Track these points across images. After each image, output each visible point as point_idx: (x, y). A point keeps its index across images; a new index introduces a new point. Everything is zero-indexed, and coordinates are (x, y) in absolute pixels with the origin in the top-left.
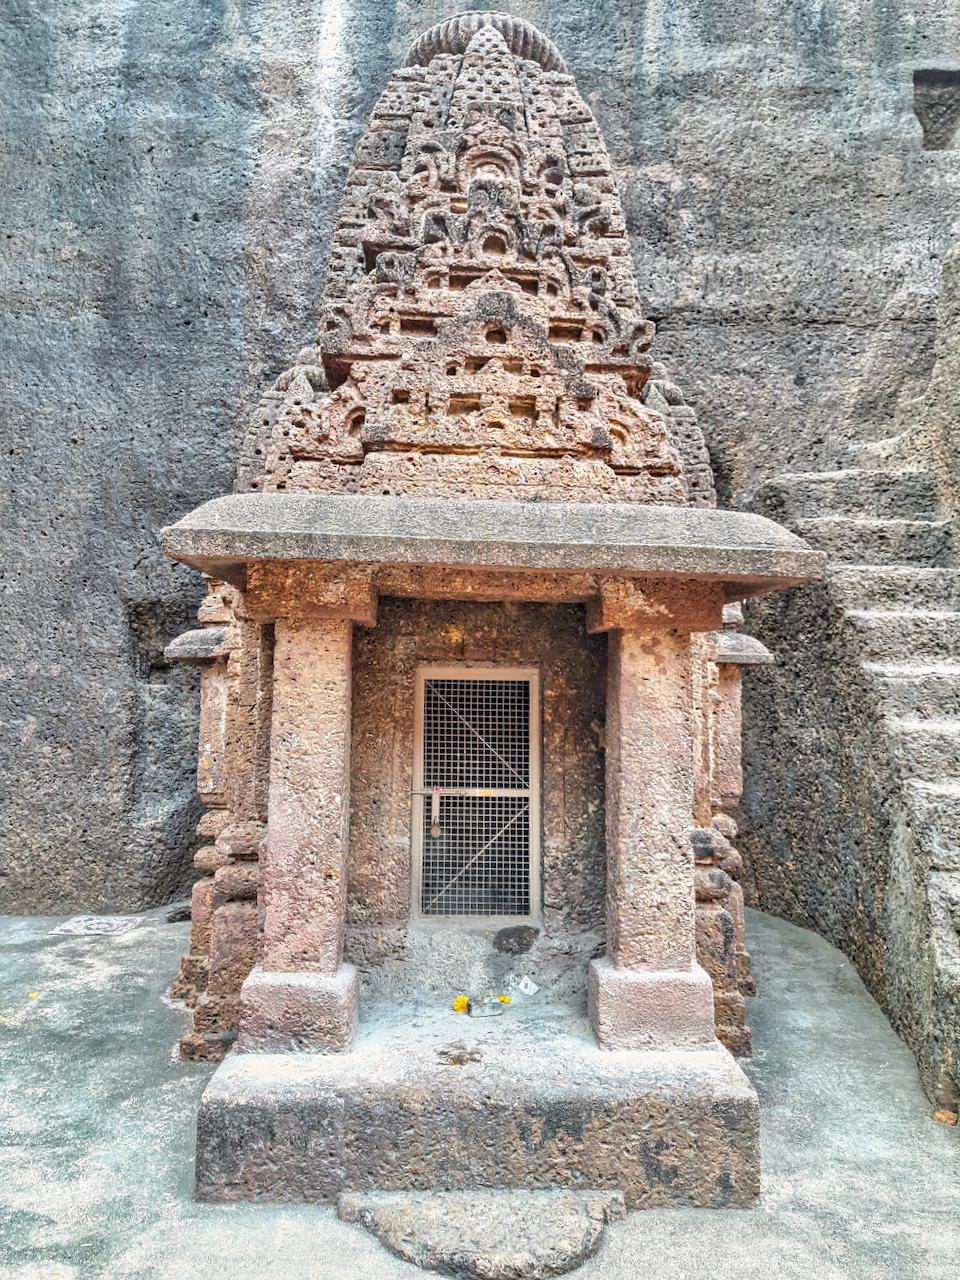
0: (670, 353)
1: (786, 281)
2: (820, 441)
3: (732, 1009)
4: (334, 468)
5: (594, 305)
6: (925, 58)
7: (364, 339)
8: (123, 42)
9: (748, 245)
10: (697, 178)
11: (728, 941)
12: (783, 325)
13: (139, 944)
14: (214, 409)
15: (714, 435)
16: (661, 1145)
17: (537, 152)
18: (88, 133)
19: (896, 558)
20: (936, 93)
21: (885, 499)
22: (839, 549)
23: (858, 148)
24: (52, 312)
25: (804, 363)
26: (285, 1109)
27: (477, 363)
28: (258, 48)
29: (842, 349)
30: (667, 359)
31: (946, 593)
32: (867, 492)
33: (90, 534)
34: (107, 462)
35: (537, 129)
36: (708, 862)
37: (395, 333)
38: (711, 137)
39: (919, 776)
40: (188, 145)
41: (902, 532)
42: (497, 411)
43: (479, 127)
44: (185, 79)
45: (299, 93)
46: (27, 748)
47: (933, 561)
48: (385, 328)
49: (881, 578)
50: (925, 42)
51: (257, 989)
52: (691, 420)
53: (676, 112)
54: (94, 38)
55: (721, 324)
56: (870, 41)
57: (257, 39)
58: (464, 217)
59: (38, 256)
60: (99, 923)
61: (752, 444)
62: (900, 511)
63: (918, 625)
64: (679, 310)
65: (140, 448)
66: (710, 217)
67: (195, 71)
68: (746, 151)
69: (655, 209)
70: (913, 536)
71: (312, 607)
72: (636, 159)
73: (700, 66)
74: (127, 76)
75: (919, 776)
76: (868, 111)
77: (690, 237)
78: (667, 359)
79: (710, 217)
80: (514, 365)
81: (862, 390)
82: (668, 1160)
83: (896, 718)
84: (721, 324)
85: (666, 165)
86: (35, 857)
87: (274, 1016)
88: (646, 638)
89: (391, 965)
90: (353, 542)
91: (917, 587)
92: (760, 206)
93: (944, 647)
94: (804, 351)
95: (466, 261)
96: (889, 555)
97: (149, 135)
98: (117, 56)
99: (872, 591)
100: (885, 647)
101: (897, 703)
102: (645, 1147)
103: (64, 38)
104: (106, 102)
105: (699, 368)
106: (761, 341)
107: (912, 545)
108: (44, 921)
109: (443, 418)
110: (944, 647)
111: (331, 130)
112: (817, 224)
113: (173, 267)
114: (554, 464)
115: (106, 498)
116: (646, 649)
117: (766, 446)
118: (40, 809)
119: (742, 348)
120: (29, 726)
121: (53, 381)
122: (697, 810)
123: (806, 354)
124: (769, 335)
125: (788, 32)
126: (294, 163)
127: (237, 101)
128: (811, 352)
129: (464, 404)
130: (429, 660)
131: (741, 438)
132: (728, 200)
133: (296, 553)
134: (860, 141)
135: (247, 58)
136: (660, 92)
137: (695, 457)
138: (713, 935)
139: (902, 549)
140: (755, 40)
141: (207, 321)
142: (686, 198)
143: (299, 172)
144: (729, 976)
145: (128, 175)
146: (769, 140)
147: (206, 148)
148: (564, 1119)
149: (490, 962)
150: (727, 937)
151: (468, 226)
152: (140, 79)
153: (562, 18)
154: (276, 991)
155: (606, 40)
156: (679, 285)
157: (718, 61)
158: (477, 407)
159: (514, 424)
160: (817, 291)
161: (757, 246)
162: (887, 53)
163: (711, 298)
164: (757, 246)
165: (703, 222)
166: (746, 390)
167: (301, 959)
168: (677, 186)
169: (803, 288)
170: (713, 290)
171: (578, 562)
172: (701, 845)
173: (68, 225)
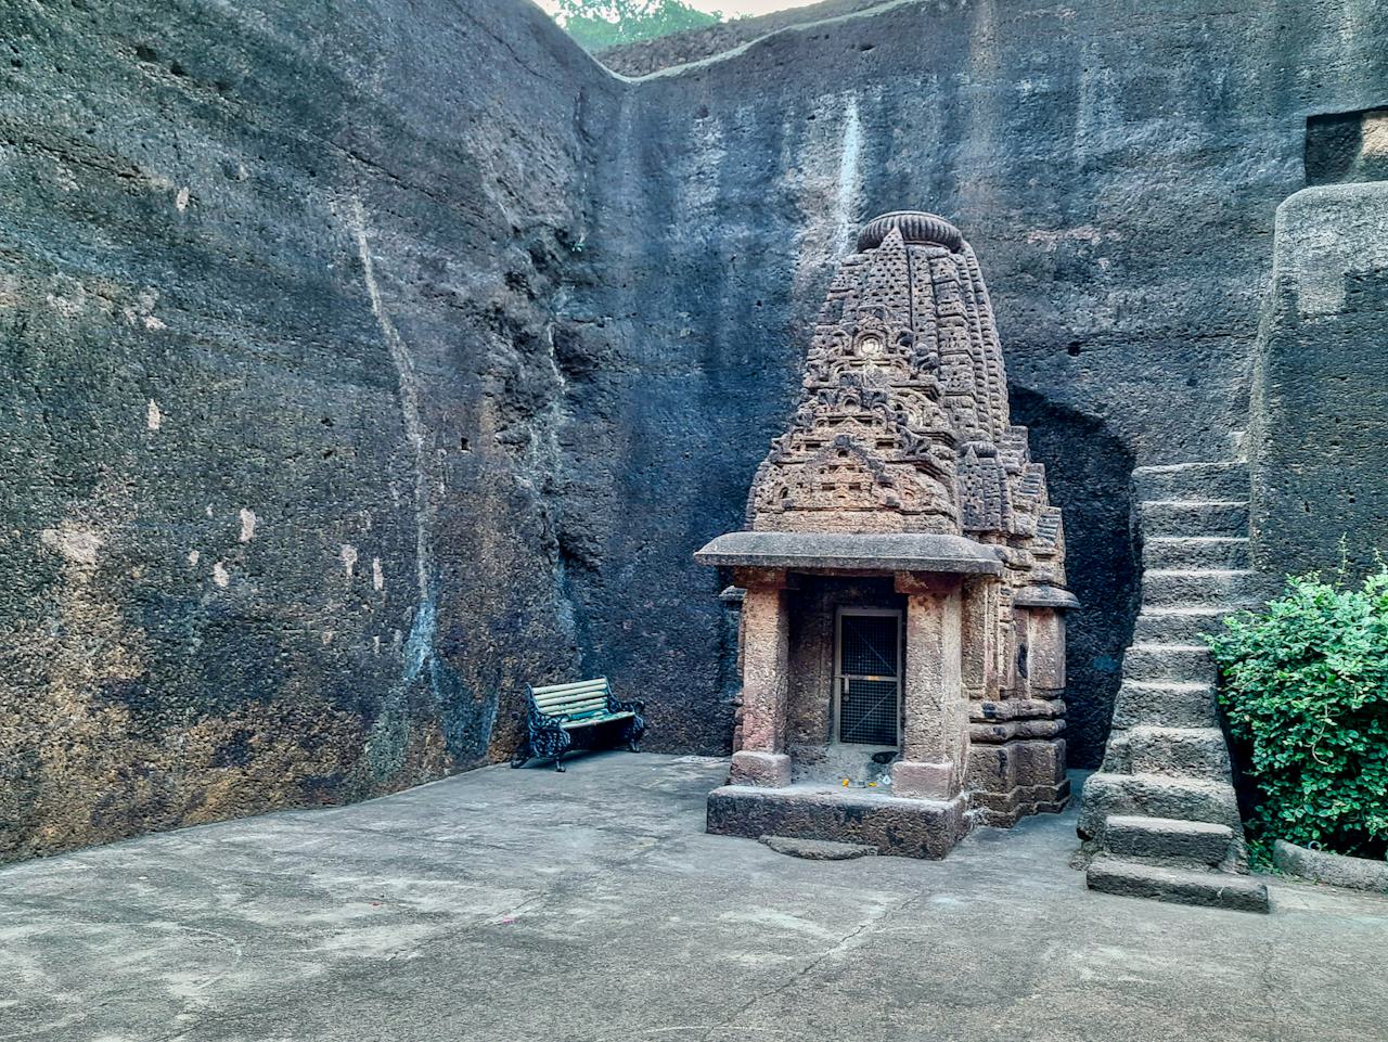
1: (1180, 308)
2: (1207, 429)
4: (774, 516)
5: (898, 430)
6: (1318, 104)
7: (789, 454)
8: (717, 183)
9: (1152, 281)
10: (1112, 234)
11: (1002, 766)
13: (717, 768)
14: (769, 430)
16: (896, 828)
17: (896, 330)
18: (696, 251)
20: (1332, 129)
21: (1213, 484)
23: (1243, 196)
24: (675, 372)
26: (740, 799)
27: (834, 468)
28: (801, 177)
29: (1228, 356)
33: (696, 515)
34: (707, 468)
35: (917, 293)
37: (803, 451)
38: (1123, 201)
40: (755, 251)
42: (843, 490)
43: (864, 320)
44: (755, 205)
45: (827, 208)
46: (660, 651)
48: (798, 449)
50: (1320, 90)
51: (738, 757)
53: (1098, 184)
54: (700, 182)
56: (1267, 98)
57: (800, 171)
58: (835, 392)
59: (667, 336)
60: (698, 759)
64: (1095, 335)
65: (725, 459)
66: (1123, 261)
67: (761, 199)
68: (1150, 209)
69: (1079, 260)
71: (761, 584)
72: (1065, 224)
73: (1118, 145)
74: (719, 206)
76: (1257, 162)
77: (1107, 278)
79: (1123, 261)
80: (851, 468)
82: (899, 835)
85: (1088, 226)
86: (664, 718)
87: (745, 770)
88: (920, 598)
89: (819, 765)
90: (769, 558)
92: (1161, 250)
95: (836, 414)
97: (732, 249)
98: (711, 194)
102: (889, 829)
103: (682, 183)
104: (706, 227)
108: (669, 756)
109: (817, 494)
111: (846, 233)
112: (1207, 259)
113: (746, 338)
114: (868, 514)
115: (704, 492)
116: (921, 604)
118: (667, 689)
120: (662, 637)
121: (675, 418)
125: (1194, 104)
126: (820, 260)
127: (787, 218)
128: (1203, 360)
129: (829, 487)
130: (844, 605)
131: (1143, 429)
132: (1136, 248)
133: (745, 563)
134: (1245, 191)
135: (793, 186)
136: (1086, 170)
140: (1166, 115)
141: (765, 372)
142: (1102, 250)
143: (824, 265)
145: (719, 277)
146: (1170, 198)
147: (767, 255)
148: (854, 813)
149: (869, 766)
151: (837, 397)
152: (727, 208)
153: (1012, 123)
154: (746, 758)
155: (1045, 134)
156: (1096, 316)
157: (1134, 138)
158: (833, 488)
159: (850, 496)
160: (1205, 313)
161: (1158, 282)
162: (1283, 103)
163: (1122, 324)
164: (1158, 282)
165: (1117, 265)
167: (757, 746)
168: (1096, 241)
169: (1194, 311)
170: (1124, 317)
171: (865, 566)
173: (684, 315)
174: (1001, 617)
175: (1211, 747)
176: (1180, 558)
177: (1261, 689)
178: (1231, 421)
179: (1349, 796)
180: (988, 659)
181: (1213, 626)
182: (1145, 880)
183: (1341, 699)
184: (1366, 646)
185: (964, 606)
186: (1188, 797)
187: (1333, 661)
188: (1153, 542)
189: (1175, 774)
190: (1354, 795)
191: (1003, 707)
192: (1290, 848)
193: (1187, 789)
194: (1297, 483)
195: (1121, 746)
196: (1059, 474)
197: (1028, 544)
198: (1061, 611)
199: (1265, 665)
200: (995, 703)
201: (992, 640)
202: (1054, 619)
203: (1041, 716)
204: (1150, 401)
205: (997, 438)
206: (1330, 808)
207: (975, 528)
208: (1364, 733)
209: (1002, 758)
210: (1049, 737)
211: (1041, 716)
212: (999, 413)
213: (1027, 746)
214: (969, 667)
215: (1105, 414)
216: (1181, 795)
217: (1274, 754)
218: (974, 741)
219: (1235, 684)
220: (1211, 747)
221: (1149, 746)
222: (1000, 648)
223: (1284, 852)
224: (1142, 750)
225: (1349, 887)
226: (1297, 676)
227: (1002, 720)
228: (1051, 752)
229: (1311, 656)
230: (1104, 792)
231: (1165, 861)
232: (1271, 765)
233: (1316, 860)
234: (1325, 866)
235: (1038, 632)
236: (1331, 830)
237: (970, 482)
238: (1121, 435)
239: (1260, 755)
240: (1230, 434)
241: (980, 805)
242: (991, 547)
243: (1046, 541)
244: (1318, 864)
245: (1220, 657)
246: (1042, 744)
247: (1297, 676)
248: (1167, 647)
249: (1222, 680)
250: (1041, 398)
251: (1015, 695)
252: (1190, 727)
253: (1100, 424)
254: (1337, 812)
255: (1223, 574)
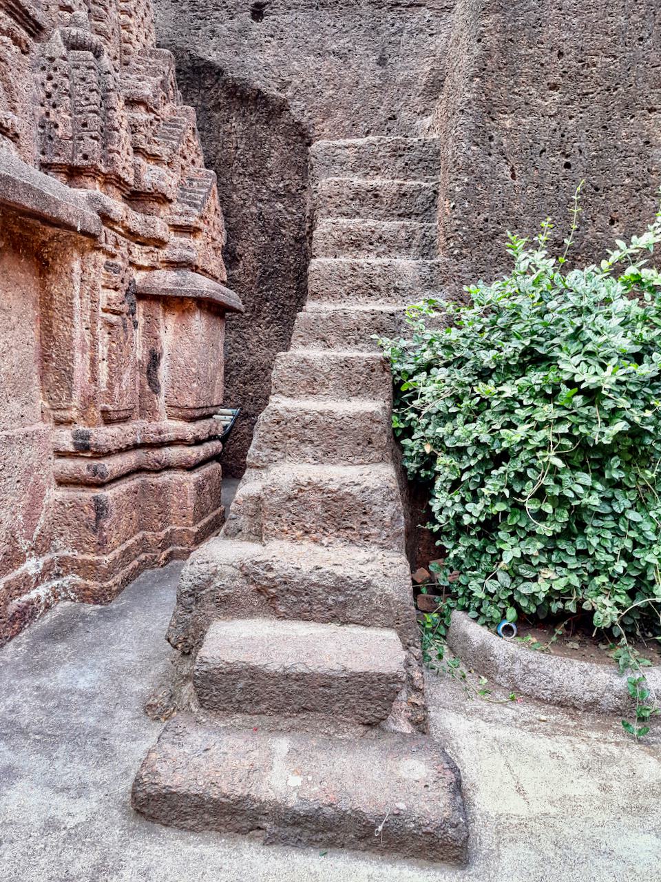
0: (272, 36)
2: (394, 118)
3: (96, 569)
11: (98, 518)
12: (371, 7)
15: (305, 112)
19: (388, 215)
21: (400, 163)
22: (338, 206)
25: (386, 44)
30: (270, 42)
31: (406, 244)
32: (384, 156)
36: (89, 455)
39: (281, 392)
41: (394, 191)
47: (421, 217)
49: (350, 230)
52: (88, 64)
55: (317, 9)
61: (337, 119)
62: (413, 174)
63: (354, 269)
70: (404, 195)
75: (281, 392)
78: (270, 42)
81: (433, 69)
83: (301, 346)
84: (317, 9)
91: (381, 238)
93: (376, 289)
94: (387, 32)
96: (381, 212)
99: (341, 241)
100: (321, 288)
101: (303, 334)
105: (296, 50)
106: (351, 24)
107: (403, 204)
110: (376, 289)
117: (348, 122)
119: (335, 30)
122: (86, 413)
123: (389, 36)
124: (358, 18)
128: (394, 34)
137: (87, 99)
138: (87, 511)
139: (394, 206)
144: (99, 544)
150: (97, 514)
166: (335, 70)
172: (80, 441)
174: (103, 303)
175: (378, 497)
176: (356, 243)
177: (453, 410)
178: (420, 108)
179: (564, 565)
180: (80, 365)
181: (390, 326)
182: (241, 800)
183: (575, 426)
184: (625, 344)
185: (43, 286)
186: (341, 586)
187: (570, 365)
188: (324, 227)
189: (325, 541)
190: (572, 563)
191: (104, 435)
192: (476, 633)
193: (339, 572)
194: (504, 140)
195: (251, 498)
196: (241, 170)
197: (164, 211)
198: (214, 308)
199: (460, 375)
200: (92, 430)
201: (88, 339)
202: (197, 316)
203: (179, 442)
204: (337, 81)
205: (126, 58)
206: (535, 579)
207: (56, 160)
208: (598, 475)
209: (100, 508)
210: (190, 468)
211: (179, 442)
212: (131, 21)
213: (155, 481)
214: (52, 378)
215: (289, 94)
216: (330, 582)
217: (463, 502)
218: (61, 483)
219: (416, 403)
220: (378, 497)
221: (290, 499)
222: (102, 350)
223: (466, 637)
224: (280, 505)
225: (560, 704)
226: (509, 390)
227: (99, 455)
228: (190, 487)
229: (533, 359)
230: (210, 582)
231: (291, 721)
232: (458, 517)
233: (513, 659)
234: (527, 671)
235: (176, 333)
236: (533, 609)
237: (49, 85)
238: (305, 120)
239: (441, 501)
240: (418, 123)
241: (67, 573)
242: (81, 193)
243: (187, 207)
244: (517, 666)
245: (397, 366)
246: (179, 476)
247: (509, 390)
248: (330, 353)
249: (400, 397)
250: (220, 72)
251: (142, 416)
252: (352, 463)
253: (283, 107)
254: (545, 587)
255: (406, 264)
